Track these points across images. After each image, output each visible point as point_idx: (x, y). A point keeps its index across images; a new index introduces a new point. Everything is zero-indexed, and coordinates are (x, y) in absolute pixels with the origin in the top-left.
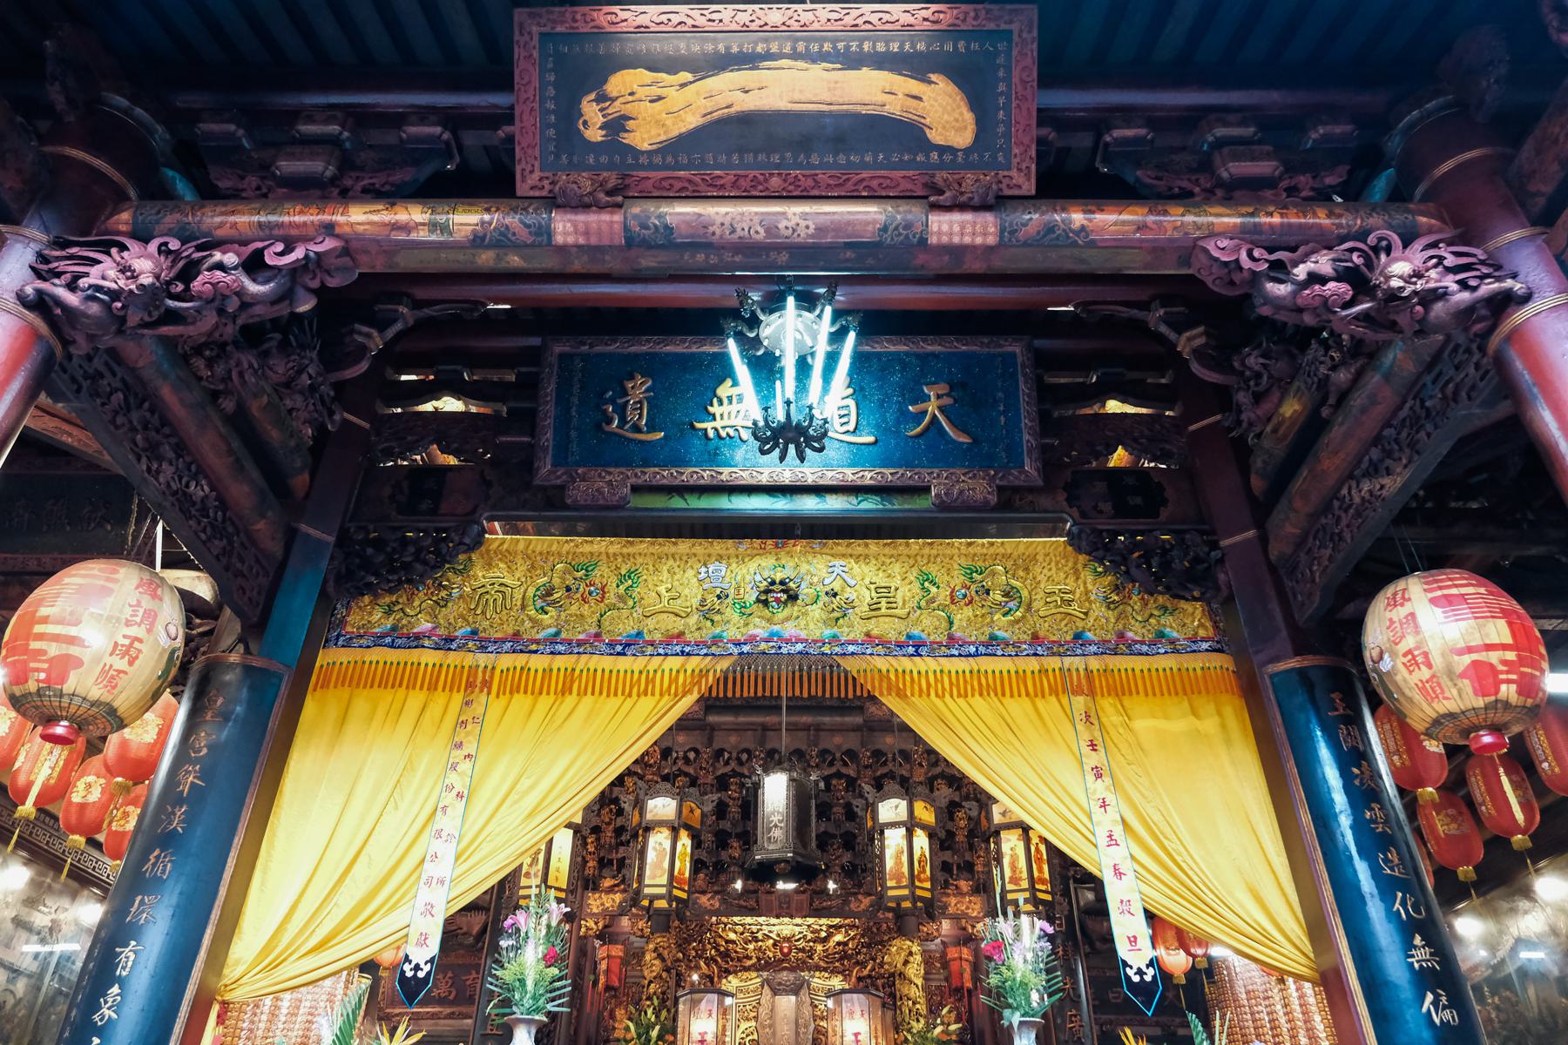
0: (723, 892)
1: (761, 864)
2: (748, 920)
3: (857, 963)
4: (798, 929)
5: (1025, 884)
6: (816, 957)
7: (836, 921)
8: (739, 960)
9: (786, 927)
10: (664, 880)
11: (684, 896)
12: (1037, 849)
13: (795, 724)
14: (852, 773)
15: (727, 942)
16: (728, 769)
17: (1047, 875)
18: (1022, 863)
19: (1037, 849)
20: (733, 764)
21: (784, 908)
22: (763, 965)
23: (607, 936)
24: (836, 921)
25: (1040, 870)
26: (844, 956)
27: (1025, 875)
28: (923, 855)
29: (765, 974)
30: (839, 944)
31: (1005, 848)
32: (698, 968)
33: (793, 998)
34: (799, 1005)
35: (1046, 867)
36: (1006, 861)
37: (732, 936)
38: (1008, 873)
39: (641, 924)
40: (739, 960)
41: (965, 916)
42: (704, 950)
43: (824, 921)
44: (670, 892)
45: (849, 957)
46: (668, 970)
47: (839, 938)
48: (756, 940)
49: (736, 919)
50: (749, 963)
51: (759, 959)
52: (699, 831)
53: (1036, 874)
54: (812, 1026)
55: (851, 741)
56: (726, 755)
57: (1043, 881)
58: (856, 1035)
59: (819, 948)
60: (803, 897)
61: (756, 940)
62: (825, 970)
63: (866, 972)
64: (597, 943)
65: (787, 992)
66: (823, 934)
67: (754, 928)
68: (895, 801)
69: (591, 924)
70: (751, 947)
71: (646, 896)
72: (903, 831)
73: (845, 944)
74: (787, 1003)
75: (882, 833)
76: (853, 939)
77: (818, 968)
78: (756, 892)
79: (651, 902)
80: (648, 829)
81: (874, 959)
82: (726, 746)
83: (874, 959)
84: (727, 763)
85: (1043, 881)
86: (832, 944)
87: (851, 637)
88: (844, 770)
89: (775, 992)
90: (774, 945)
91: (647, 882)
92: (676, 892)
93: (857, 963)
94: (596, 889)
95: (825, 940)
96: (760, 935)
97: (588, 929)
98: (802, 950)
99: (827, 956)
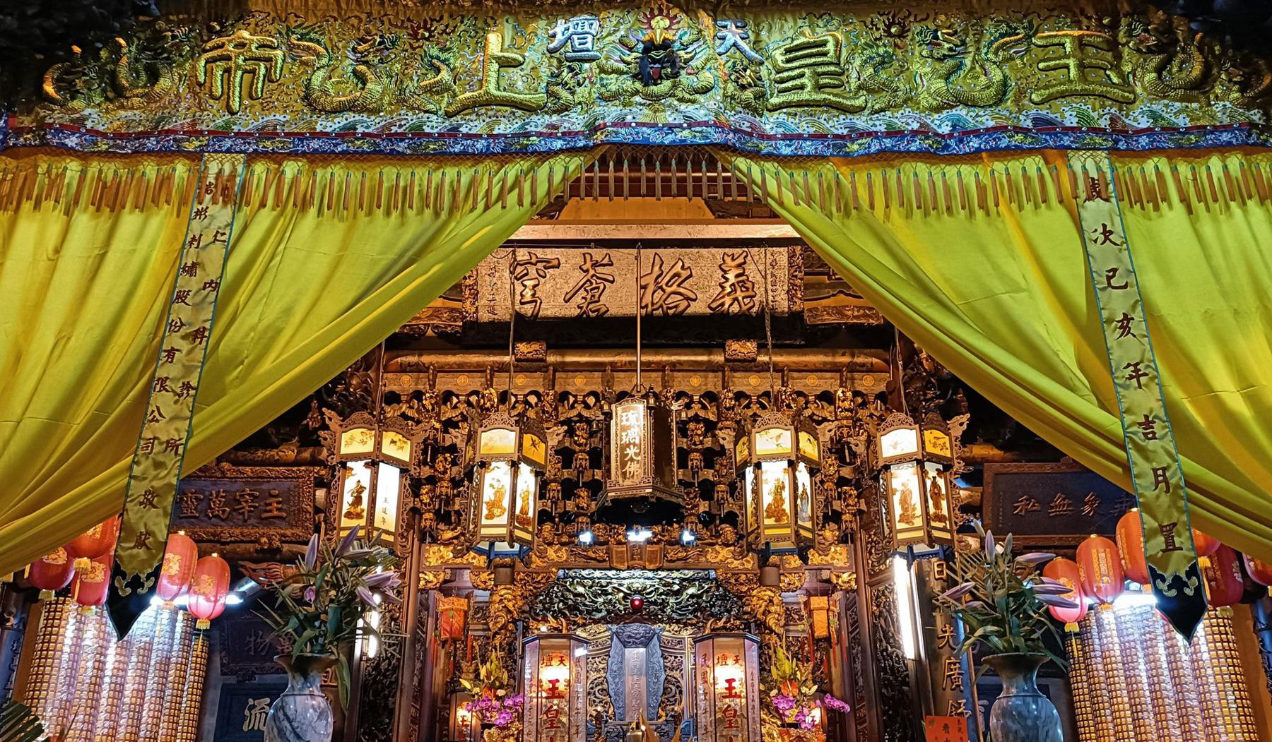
0: (572, 542)
1: (614, 501)
2: (597, 574)
3: (712, 615)
4: (648, 582)
5: (918, 522)
6: (668, 611)
7: (690, 573)
8: (589, 613)
9: (636, 579)
10: (504, 519)
11: (528, 537)
12: (934, 484)
13: (649, 364)
14: (712, 418)
15: (576, 595)
16: (573, 413)
17: (945, 512)
18: (916, 499)
19: (934, 484)
20: (579, 407)
21: (635, 559)
22: (614, 617)
23: (446, 589)
24: (690, 573)
25: (937, 506)
26: (698, 608)
27: (918, 512)
28: (804, 491)
29: (614, 628)
30: (692, 596)
31: (896, 484)
32: (545, 620)
33: (643, 650)
34: (649, 655)
35: (944, 503)
36: (896, 499)
37: (581, 589)
38: (898, 511)
39: (484, 576)
40: (589, 613)
41: (829, 567)
42: (552, 603)
43: (676, 574)
44: (511, 533)
45: (703, 610)
46: (515, 622)
47: (692, 591)
48: (605, 593)
49: (584, 573)
50: (599, 615)
51: (609, 612)
52: (544, 467)
53: (932, 510)
54: (663, 677)
55: (712, 382)
56: (572, 399)
57: (940, 518)
58: (730, 681)
59: (672, 600)
60: (655, 547)
61: (605, 593)
62: (678, 622)
63: (720, 624)
64: (440, 596)
65: (636, 645)
66: (676, 587)
67: (604, 582)
68: (774, 432)
69: (430, 577)
70: (601, 600)
71: (484, 538)
72: (785, 464)
73: (700, 596)
74: (635, 655)
75: (758, 466)
76: (707, 592)
77: (670, 620)
78: (606, 543)
79: (492, 545)
80: (483, 465)
81: (729, 611)
82: (569, 389)
83: (729, 611)
84: (573, 407)
85: (940, 518)
86: (684, 596)
87: (776, 114)
88: (702, 414)
89: (625, 645)
90: (625, 598)
91: (484, 522)
92: (518, 533)
93: (712, 615)
94: (435, 540)
95: (677, 593)
96: (609, 589)
97: (427, 582)
98: (655, 603)
99: (680, 608)
